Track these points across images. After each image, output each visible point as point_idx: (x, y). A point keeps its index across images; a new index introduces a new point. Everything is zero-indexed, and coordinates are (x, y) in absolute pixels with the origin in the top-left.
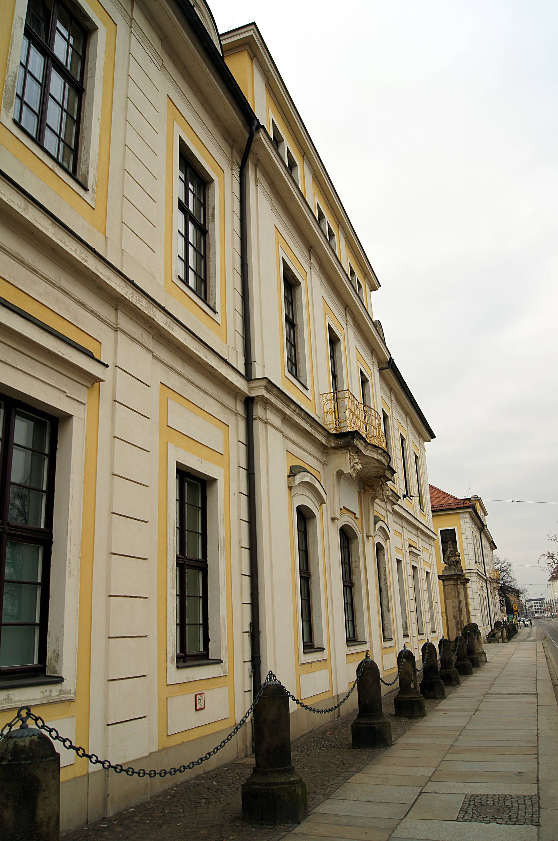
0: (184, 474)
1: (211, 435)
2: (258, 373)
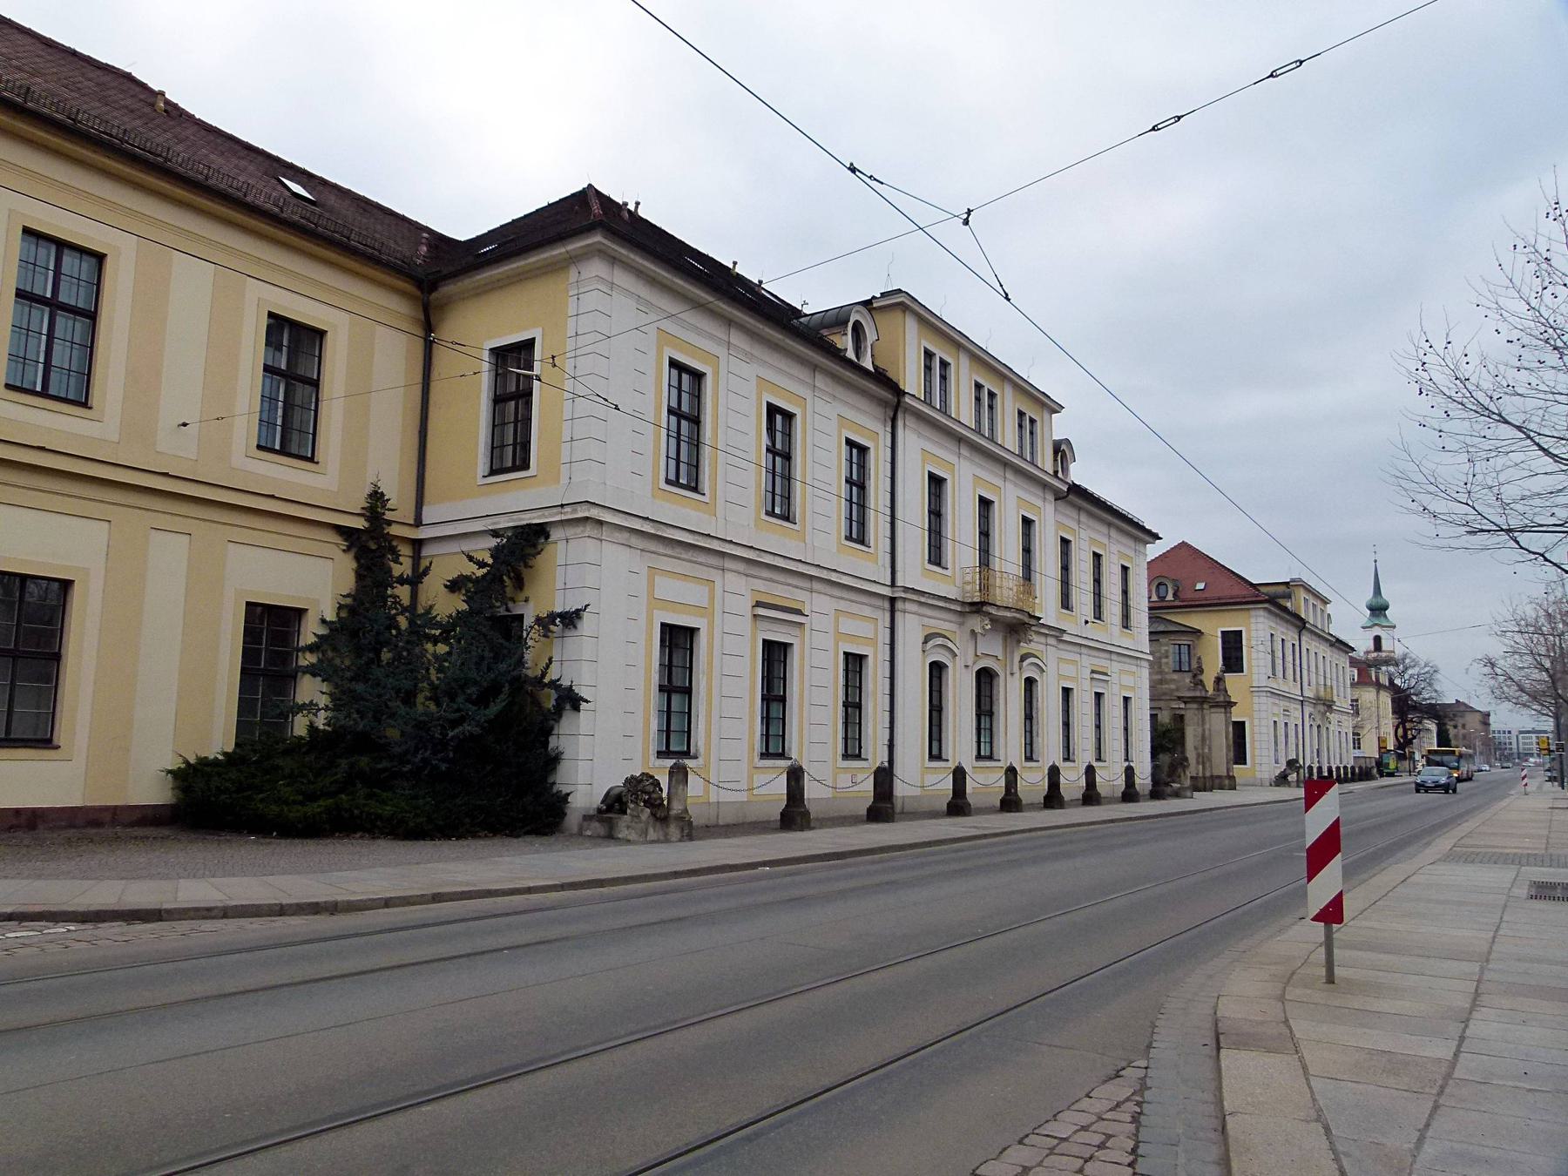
0: (932, 477)
1: (865, 629)
2: (899, 583)
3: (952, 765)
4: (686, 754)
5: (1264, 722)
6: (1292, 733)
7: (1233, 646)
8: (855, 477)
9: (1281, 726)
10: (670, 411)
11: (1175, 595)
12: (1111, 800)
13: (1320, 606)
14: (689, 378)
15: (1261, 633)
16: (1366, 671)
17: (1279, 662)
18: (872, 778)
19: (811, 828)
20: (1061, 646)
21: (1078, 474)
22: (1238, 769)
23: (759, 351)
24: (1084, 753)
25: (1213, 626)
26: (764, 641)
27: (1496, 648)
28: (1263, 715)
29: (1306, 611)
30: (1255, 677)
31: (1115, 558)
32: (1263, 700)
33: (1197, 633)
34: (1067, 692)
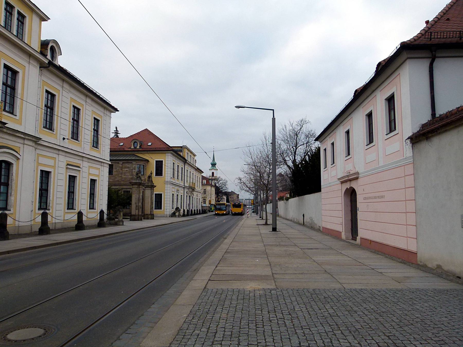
3: (77, 211)
4: (46, 209)
5: (169, 194)
6: (179, 198)
7: (159, 165)
8: (49, 105)
9: (175, 195)
10: (45, 106)
11: (140, 147)
12: (92, 227)
13: (192, 156)
14: (51, 96)
15: (169, 162)
16: (208, 181)
17: (176, 173)
18: (41, 216)
19: (8, 239)
20: (39, 147)
21: (61, 61)
22: (156, 212)
23: (73, 90)
24: (191, 208)
25: (153, 159)
26: (69, 176)
27: (242, 175)
28: (168, 191)
29: (188, 157)
30: (166, 178)
31: (90, 113)
32: (169, 186)
33: (148, 161)
34: (93, 182)
